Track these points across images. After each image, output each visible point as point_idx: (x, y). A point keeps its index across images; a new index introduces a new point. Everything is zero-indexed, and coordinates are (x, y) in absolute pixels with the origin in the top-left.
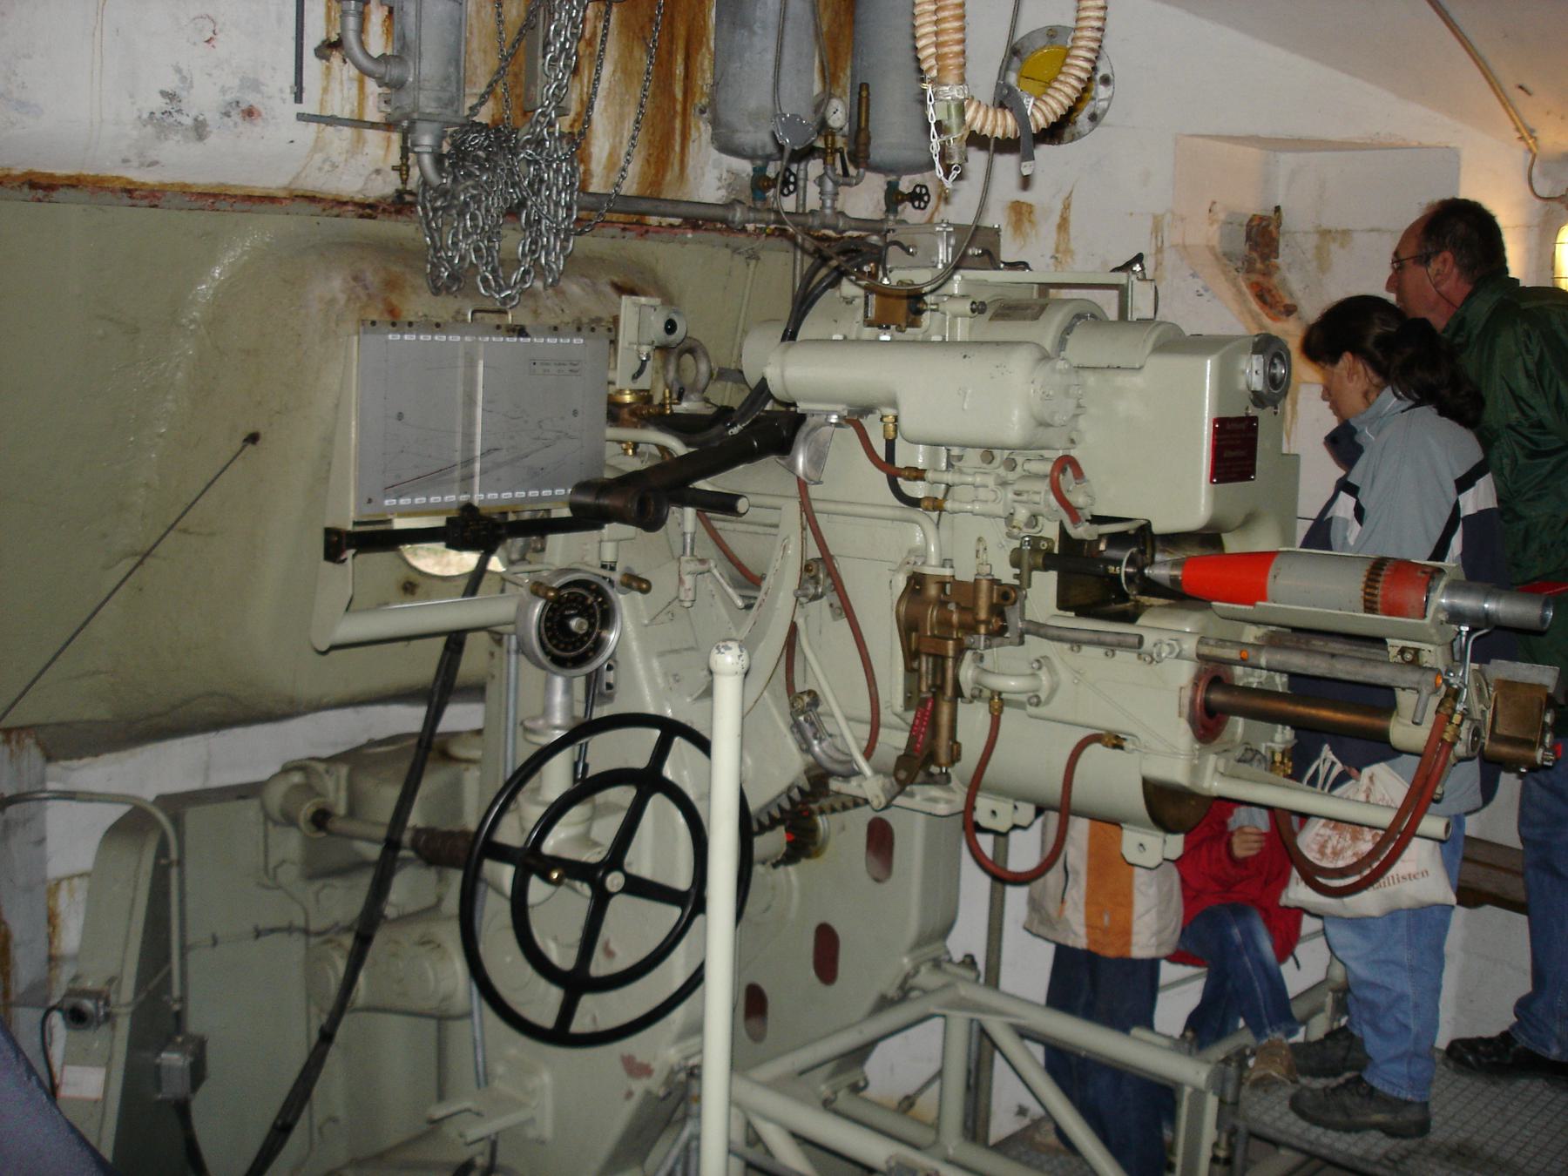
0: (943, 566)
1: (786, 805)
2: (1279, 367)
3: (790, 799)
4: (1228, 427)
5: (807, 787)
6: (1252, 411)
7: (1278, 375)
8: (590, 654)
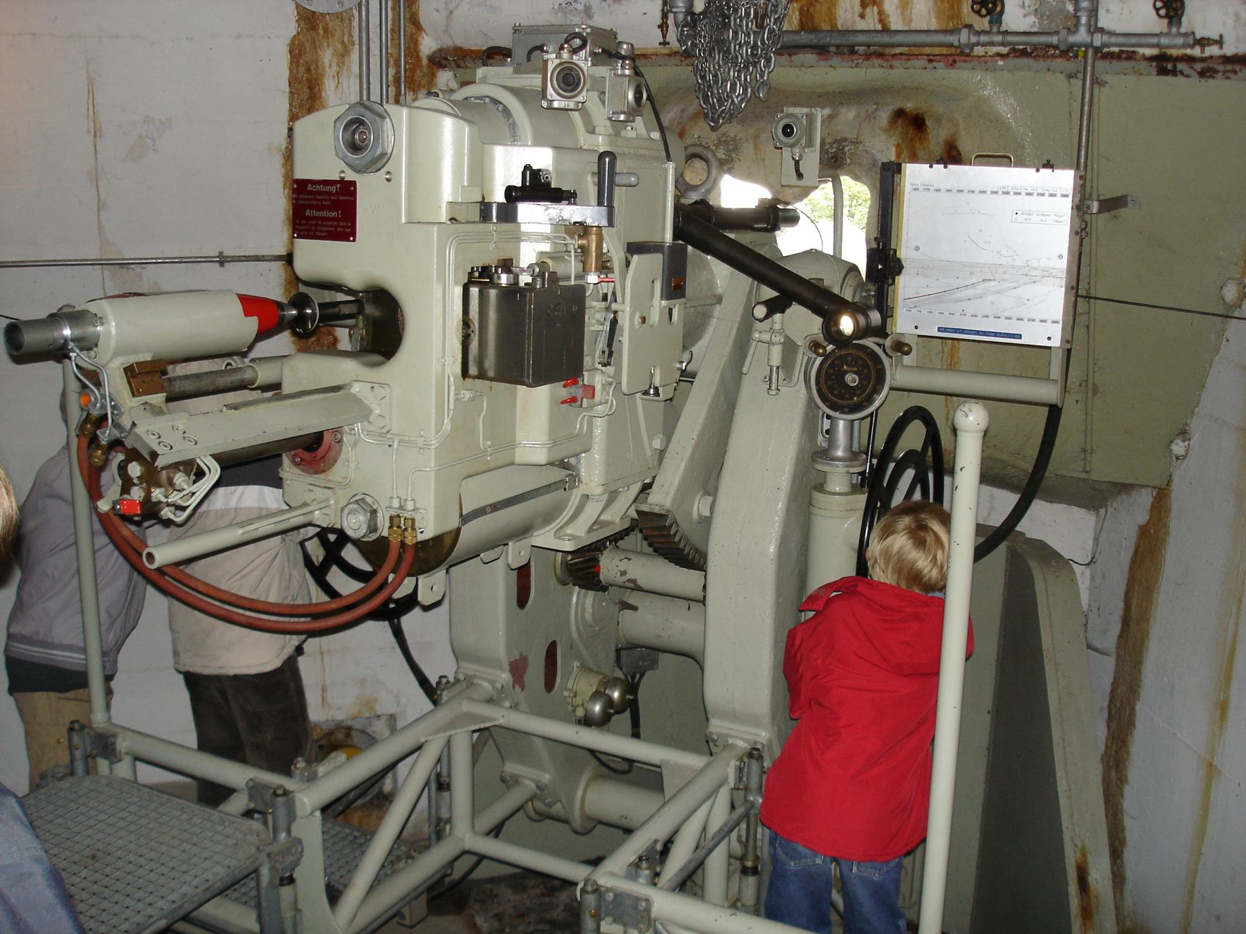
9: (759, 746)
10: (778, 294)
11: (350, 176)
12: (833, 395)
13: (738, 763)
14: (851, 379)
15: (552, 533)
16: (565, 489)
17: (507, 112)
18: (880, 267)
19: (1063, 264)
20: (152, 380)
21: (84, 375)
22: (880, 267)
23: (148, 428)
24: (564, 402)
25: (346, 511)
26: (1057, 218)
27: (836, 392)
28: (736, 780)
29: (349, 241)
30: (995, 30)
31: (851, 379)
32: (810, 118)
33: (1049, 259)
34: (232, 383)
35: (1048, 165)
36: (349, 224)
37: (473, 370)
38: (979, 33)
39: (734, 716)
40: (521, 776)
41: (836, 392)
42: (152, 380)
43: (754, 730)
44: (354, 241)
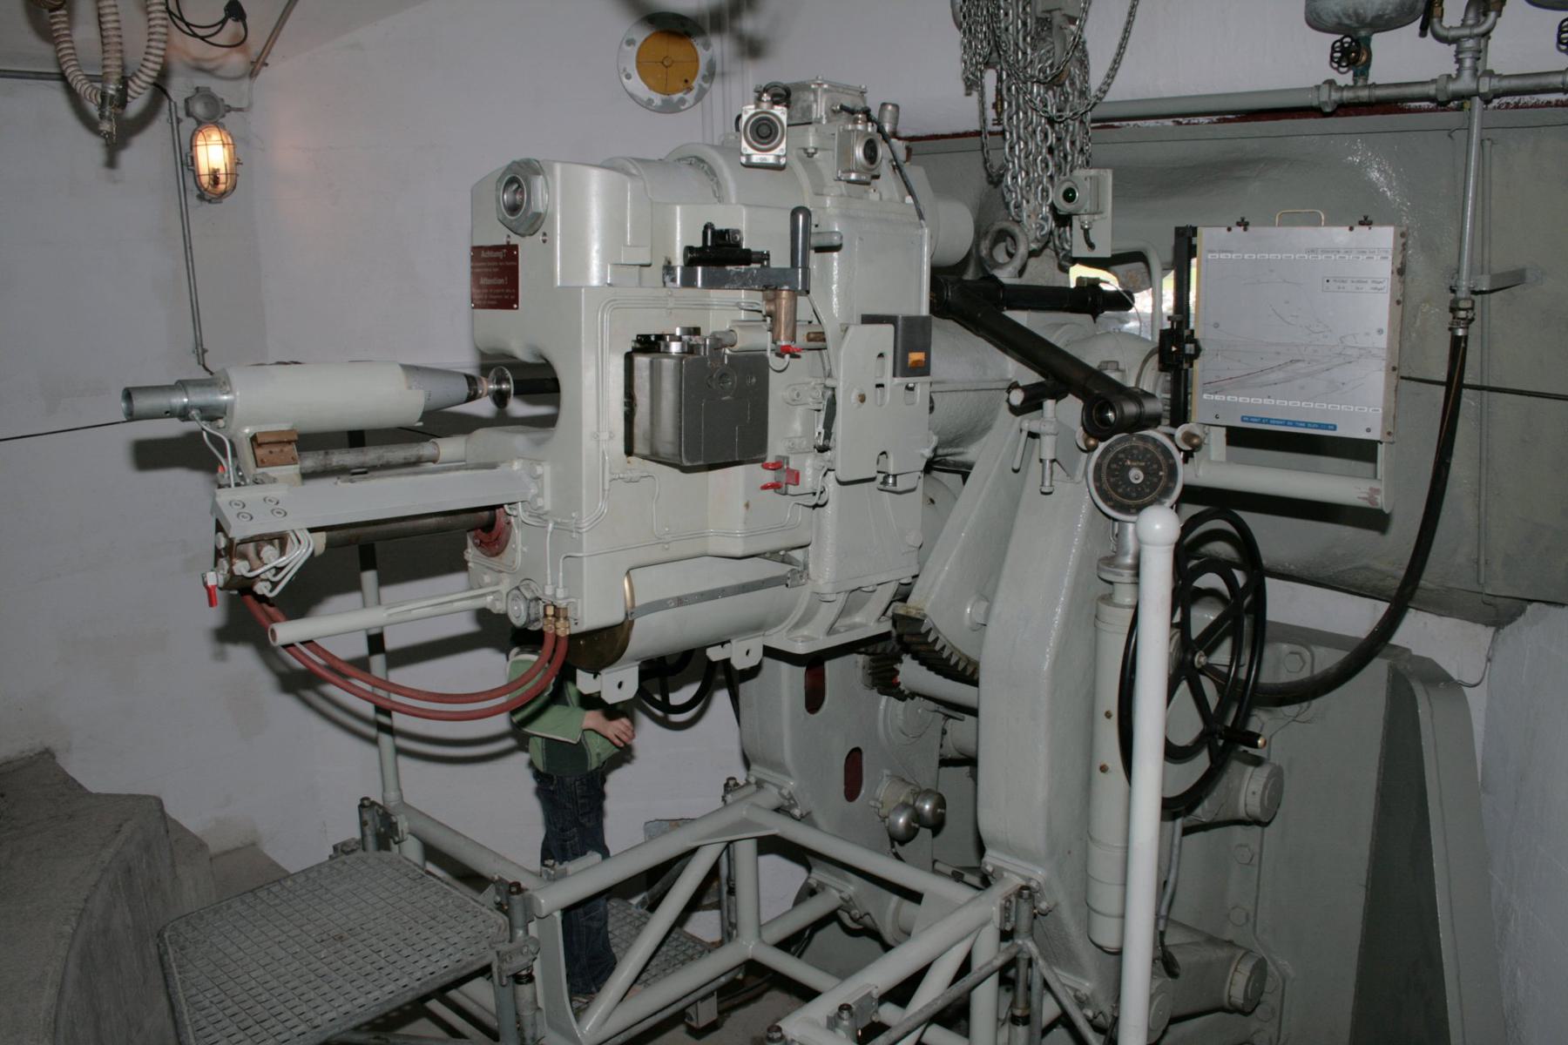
9: (1033, 884)
10: (1041, 379)
11: (515, 240)
12: (1117, 493)
13: (1003, 902)
14: (1136, 475)
15: (784, 631)
16: (787, 585)
17: (711, 173)
18: (1174, 349)
19: (1382, 342)
20: (282, 451)
21: (212, 443)
22: (1174, 349)
23: (265, 494)
24: (765, 487)
25: (510, 597)
26: (1374, 285)
27: (1120, 490)
28: (1001, 920)
29: (513, 308)
30: (1360, 83)
31: (1136, 475)
32: (1096, 182)
33: (1367, 334)
34: (405, 459)
35: (1366, 222)
36: (514, 291)
37: (640, 446)
38: (1341, 89)
39: (1009, 849)
40: (827, 885)
41: (1120, 490)
42: (282, 451)
43: (1031, 867)
44: (517, 308)
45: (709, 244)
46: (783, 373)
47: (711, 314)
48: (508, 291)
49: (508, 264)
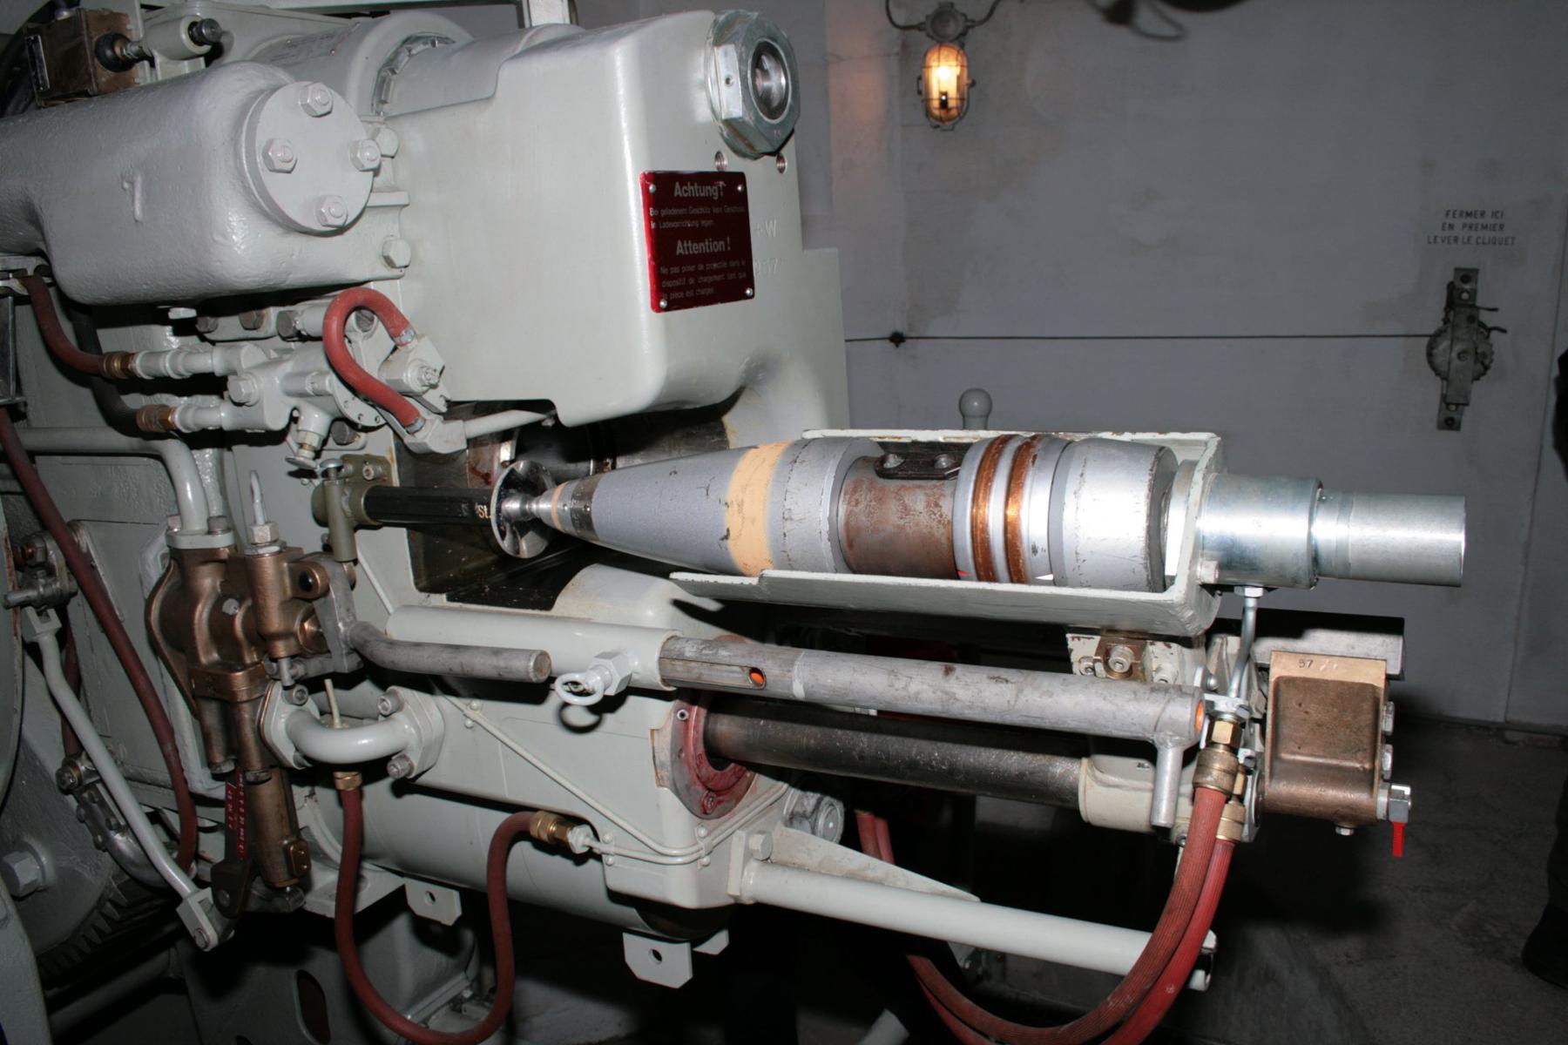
0: (210, 532)
1: (103, 925)
2: (773, 74)
3: (106, 917)
4: (678, 191)
5: (124, 901)
6: (731, 163)
7: (775, 90)
8: (760, 376)
45: (241, 775)
46: (1425, 363)
47: (269, 536)
48: (733, 264)
49: (729, 210)
